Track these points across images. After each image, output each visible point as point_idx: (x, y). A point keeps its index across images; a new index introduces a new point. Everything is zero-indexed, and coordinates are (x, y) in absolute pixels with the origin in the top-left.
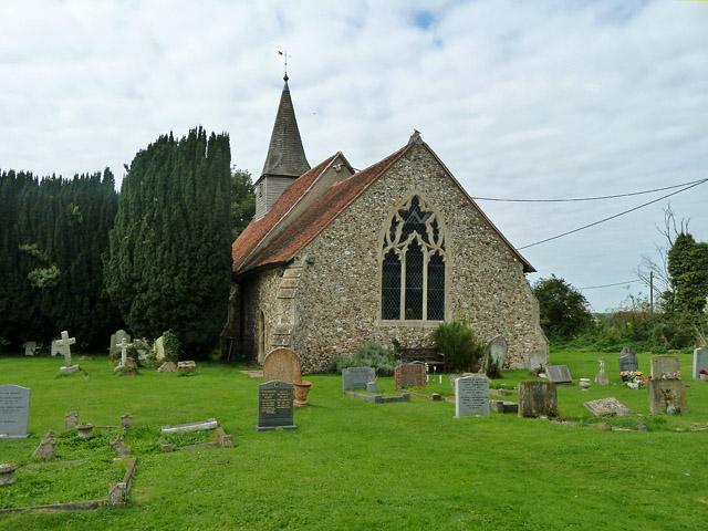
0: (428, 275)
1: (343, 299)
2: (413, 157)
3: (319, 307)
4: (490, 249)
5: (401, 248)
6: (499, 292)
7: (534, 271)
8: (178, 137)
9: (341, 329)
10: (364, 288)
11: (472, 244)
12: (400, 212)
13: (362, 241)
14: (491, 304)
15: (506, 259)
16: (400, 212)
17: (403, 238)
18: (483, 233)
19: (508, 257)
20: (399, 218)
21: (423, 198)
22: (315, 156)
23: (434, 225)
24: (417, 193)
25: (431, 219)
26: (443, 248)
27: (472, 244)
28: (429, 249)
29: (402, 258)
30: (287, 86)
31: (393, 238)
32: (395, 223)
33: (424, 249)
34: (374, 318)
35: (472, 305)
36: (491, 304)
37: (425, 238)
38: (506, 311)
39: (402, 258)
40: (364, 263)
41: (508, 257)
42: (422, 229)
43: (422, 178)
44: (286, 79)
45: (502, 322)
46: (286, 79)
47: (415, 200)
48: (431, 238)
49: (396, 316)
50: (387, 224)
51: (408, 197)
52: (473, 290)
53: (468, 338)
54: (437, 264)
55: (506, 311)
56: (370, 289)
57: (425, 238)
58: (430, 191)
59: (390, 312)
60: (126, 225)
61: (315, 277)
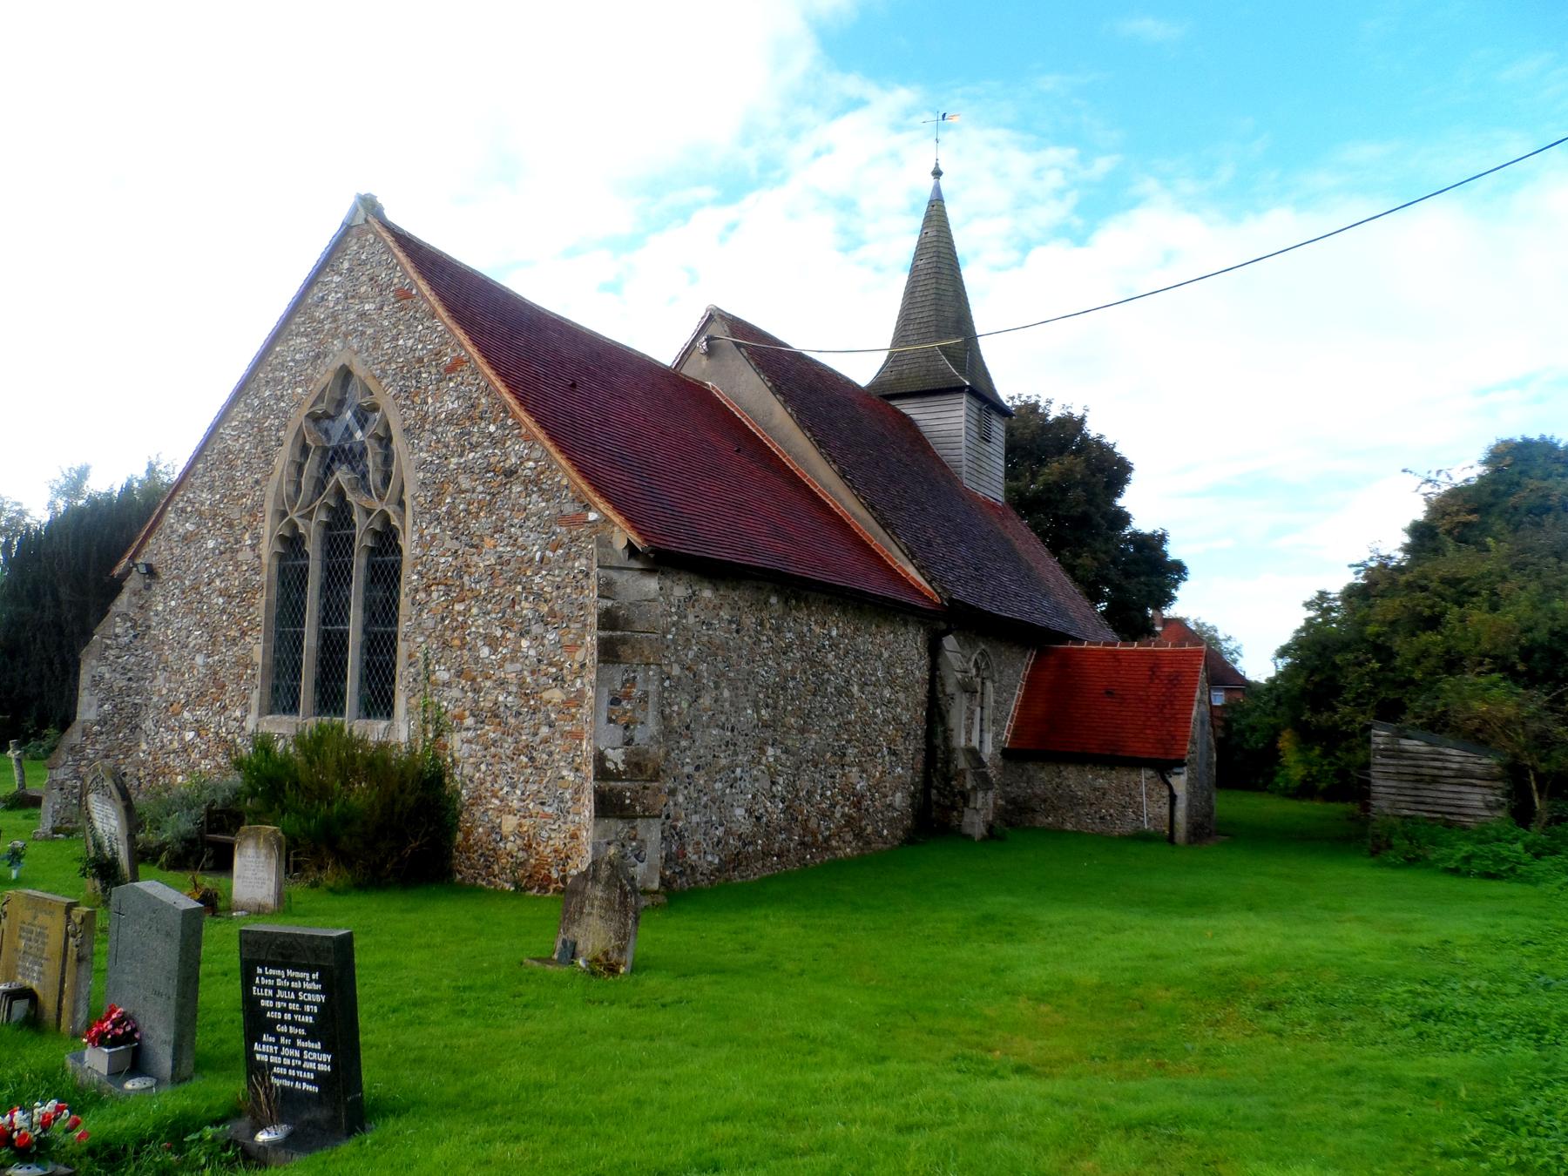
1: (199, 659)
6: (536, 629)
7: (628, 540)
10: (234, 633)
11: (465, 483)
13: (235, 515)
15: (562, 519)
17: (320, 485)
18: (495, 442)
19: (569, 509)
21: (359, 370)
24: (343, 359)
27: (465, 483)
28: (369, 512)
30: (937, 190)
34: (247, 710)
35: (460, 674)
38: (556, 695)
41: (569, 509)
43: (363, 315)
44: (937, 173)
45: (544, 730)
46: (937, 173)
47: (345, 375)
48: (374, 478)
52: (463, 625)
54: (386, 539)
55: (556, 695)
56: (244, 633)
59: (282, 699)
60: (1128, 959)
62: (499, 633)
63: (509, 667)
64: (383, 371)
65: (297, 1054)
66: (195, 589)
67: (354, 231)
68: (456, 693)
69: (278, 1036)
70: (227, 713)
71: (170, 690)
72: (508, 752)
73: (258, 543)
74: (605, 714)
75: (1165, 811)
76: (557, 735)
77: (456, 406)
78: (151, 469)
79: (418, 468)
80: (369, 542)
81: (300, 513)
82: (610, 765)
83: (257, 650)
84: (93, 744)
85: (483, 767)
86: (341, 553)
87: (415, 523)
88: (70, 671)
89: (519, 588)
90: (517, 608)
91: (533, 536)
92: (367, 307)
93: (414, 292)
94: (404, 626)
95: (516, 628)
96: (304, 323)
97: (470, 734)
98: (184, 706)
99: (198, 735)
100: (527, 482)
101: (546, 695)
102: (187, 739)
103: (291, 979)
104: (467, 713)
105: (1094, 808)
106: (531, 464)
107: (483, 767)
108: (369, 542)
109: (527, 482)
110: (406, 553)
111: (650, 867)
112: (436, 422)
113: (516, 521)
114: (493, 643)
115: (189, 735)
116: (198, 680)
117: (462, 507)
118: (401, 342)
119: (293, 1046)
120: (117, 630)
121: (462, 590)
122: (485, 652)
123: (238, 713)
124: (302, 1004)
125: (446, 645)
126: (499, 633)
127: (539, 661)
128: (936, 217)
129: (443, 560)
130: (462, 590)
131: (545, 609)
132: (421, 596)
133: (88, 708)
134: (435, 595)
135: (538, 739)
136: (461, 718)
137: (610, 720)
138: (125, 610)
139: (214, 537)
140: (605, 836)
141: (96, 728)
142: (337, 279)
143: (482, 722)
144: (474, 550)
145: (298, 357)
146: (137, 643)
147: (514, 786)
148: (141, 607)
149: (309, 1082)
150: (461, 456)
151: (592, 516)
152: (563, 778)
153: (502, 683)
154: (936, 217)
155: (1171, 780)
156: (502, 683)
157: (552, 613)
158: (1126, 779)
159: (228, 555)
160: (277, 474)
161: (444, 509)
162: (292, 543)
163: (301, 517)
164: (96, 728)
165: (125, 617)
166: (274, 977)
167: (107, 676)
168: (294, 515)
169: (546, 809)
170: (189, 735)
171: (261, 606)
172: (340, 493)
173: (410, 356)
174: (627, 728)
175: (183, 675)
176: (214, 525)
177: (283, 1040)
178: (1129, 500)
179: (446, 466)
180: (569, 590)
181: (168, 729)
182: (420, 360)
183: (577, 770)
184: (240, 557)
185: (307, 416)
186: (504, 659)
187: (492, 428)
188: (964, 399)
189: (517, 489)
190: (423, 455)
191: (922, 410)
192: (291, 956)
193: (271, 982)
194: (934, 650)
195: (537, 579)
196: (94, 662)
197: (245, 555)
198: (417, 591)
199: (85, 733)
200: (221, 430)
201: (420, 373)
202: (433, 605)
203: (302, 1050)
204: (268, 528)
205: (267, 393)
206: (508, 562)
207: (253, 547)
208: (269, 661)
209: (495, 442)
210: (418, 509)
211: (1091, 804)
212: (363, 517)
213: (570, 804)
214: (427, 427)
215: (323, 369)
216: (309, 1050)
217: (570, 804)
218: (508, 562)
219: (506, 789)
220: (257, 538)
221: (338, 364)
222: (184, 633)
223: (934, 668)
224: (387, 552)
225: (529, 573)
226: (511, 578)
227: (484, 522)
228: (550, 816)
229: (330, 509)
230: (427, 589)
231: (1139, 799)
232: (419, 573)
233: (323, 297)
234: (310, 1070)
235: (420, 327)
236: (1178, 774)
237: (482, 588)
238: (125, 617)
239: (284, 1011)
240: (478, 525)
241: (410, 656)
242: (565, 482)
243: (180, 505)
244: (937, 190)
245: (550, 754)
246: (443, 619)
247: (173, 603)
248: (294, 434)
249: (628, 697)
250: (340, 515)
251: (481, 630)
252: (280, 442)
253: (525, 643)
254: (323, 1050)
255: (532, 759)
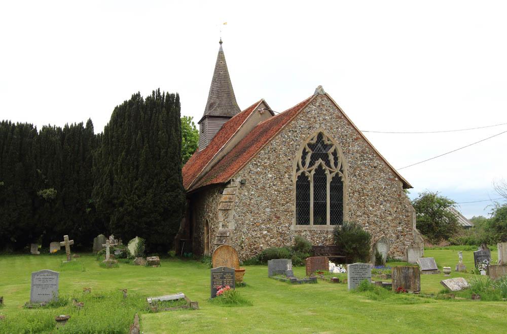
6: (384, 203)
15: (389, 179)
18: (371, 160)
21: (326, 133)
22: (244, 102)
23: (335, 154)
30: (221, 48)
32: (305, 153)
42: (325, 158)
44: (221, 43)
47: (320, 135)
49: (307, 222)
50: (299, 155)
51: (314, 134)
59: (302, 219)
63: (378, 212)
68: (363, 218)
78: (26, 123)
114: (373, 206)
122: (371, 208)
126: (374, 204)
128: (221, 56)
136: (364, 224)
154: (221, 56)
170: (265, 232)
200: (272, 142)
209: (371, 160)
221: (319, 132)
230: (353, 193)
253: (381, 206)
255: (384, 232)
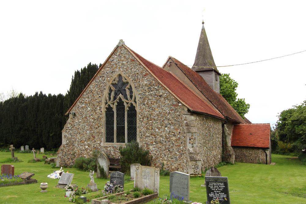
0: (128, 118)
1: (88, 132)
2: (118, 54)
3: (78, 135)
4: (163, 99)
5: (113, 104)
6: (169, 126)
7: (90, 63)
8: (33, 96)
9: (87, 147)
10: (96, 126)
11: (150, 98)
12: (113, 84)
13: (95, 103)
14: (163, 134)
15: (173, 105)
16: (113, 84)
17: (115, 98)
18: (157, 90)
20: (113, 88)
23: (130, 89)
24: (120, 73)
25: (128, 86)
26: (136, 102)
27: (150, 98)
28: (127, 103)
29: (115, 110)
30: (203, 27)
31: (110, 98)
32: (111, 90)
33: (125, 104)
34: (101, 142)
35: (152, 134)
36: (163, 134)
37: (126, 97)
38: (174, 138)
39: (115, 110)
40: (96, 113)
41: (175, 103)
43: (123, 64)
45: (171, 145)
46: (203, 23)
47: (120, 76)
48: (129, 97)
49: (112, 141)
50: (106, 92)
51: (115, 75)
52: (152, 125)
53: (147, 153)
54: (132, 110)
56: (99, 127)
57: (126, 97)
58: (127, 70)
59: (109, 139)
61: (77, 122)
62: (160, 127)
64: (129, 75)
65: (219, 195)
66: (86, 118)
67: (119, 47)
68: (151, 138)
69: (214, 193)
70: (96, 142)
71: (81, 138)
72: (164, 149)
73: (101, 109)
74: (189, 142)
75: (265, 158)
76: (174, 146)
77: (147, 83)
79: (139, 94)
80: (128, 109)
81: (111, 103)
82: (190, 151)
83: (103, 130)
84: (65, 149)
85: (158, 152)
86: (121, 111)
87: (139, 105)
88: (61, 134)
89: (164, 118)
90: (164, 122)
91: (167, 108)
92: (124, 62)
93: (135, 60)
94: (138, 125)
95: (164, 126)
96: (108, 65)
97: (155, 146)
98: (85, 141)
99: (89, 147)
100: (165, 98)
101: (172, 138)
102: (86, 147)
103: (217, 184)
104: (154, 142)
105: (250, 157)
106: (165, 94)
107: (158, 152)
108: (128, 109)
109: (165, 98)
110: (137, 111)
111: (200, 170)
112: (143, 85)
113: (163, 105)
114: (159, 129)
115: (87, 147)
116: (88, 136)
117: (150, 102)
118: (133, 70)
119: (218, 194)
120: (69, 126)
121: (151, 118)
122: (157, 130)
123: (99, 142)
124: (220, 187)
125: (148, 129)
126: (160, 127)
127: (170, 132)
128: (203, 32)
129: (146, 113)
130: (151, 118)
131: (170, 122)
132: (141, 119)
133: (64, 142)
134: (145, 119)
135: (170, 147)
136: (152, 143)
137: (189, 143)
138: (70, 122)
139: (90, 108)
140: (192, 164)
141: (66, 146)
142: (116, 56)
143: (157, 144)
144: (153, 111)
145: (108, 72)
146: (73, 128)
147: (165, 156)
148: (73, 121)
149: (221, 199)
150: (149, 92)
151: (180, 104)
152: (176, 154)
153: (161, 136)
154: (203, 32)
155: (266, 152)
156: (161, 136)
157: (172, 123)
158: (256, 151)
159: (94, 111)
160: (104, 95)
161: (146, 103)
162: (109, 110)
163: (111, 104)
164: (66, 146)
165: (70, 123)
166: (214, 184)
167: (67, 135)
168: (109, 103)
169: (173, 160)
170: (87, 147)
171: (104, 120)
172: (120, 99)
173: (135, 73)
174: (192, 144)
175: (84, 135)
176: (90, 105)
177: (215, 193)
178: (237, 91)
179: (146, 94)
180: (175, 118)
181: (81, 146)
182: (138, 73)
183: (179, 152)
184: (97, 112)
185: (111, 84)
186: (162, 131)
187: (156, 87)
188: (213, 72)
189: (163, 99)
190: (140, 92)
191: (203, 75)
192: (217, 181)
193: (213, 185)
194: (223, 126)
195: (168, 116)
196: (64, 133)
197: (98, 111)
198: (140, 118)
199: (64, 147)
200: (90, 86)
201: (138, 76)
202: (144, 121)
203: (220, 194)
204: (103, 106)
205: (101, 79)
206: (161, 113)
207: (100, 110)
208: (105, 132)
209: (157, 90)
210: (139, 103)
211: (249, 157)
212: (126, 104)
213: (178, 158)
214: (140, 87)
215: (114, 75)
216: (221, 194)
217: (178, 158)
218: (161, 113)
219: (163, 156)
220: (101, 108)
222: (83, 127)
223: (223, 130)
224: (132, 111)
225: (166, 115)
226: (162, 116)
227: (155, 106)
228: (174, 161)
229: (118, 102)
230: (143, 118)
231: (259, 156)
232: (141, 115)
233: (113, 60)
234: (222, 197)
235: (137, 67)
236: (268, 150)
237: (156, 118)
238: (70, 123)
239: (215, 189)
240: (155, 106)
241: (140, 131)
242: (173, 98)
243: (81, 101)
244: (203, 27)
245: (173, 149)
246: (147, 124)
247: (80, 121)
248: (108, 87)
249: (192, 139)
250: (120, 105)
251: (156, 126)
252: (105, 89)
254: (225, 194)
255: (169, 150)
